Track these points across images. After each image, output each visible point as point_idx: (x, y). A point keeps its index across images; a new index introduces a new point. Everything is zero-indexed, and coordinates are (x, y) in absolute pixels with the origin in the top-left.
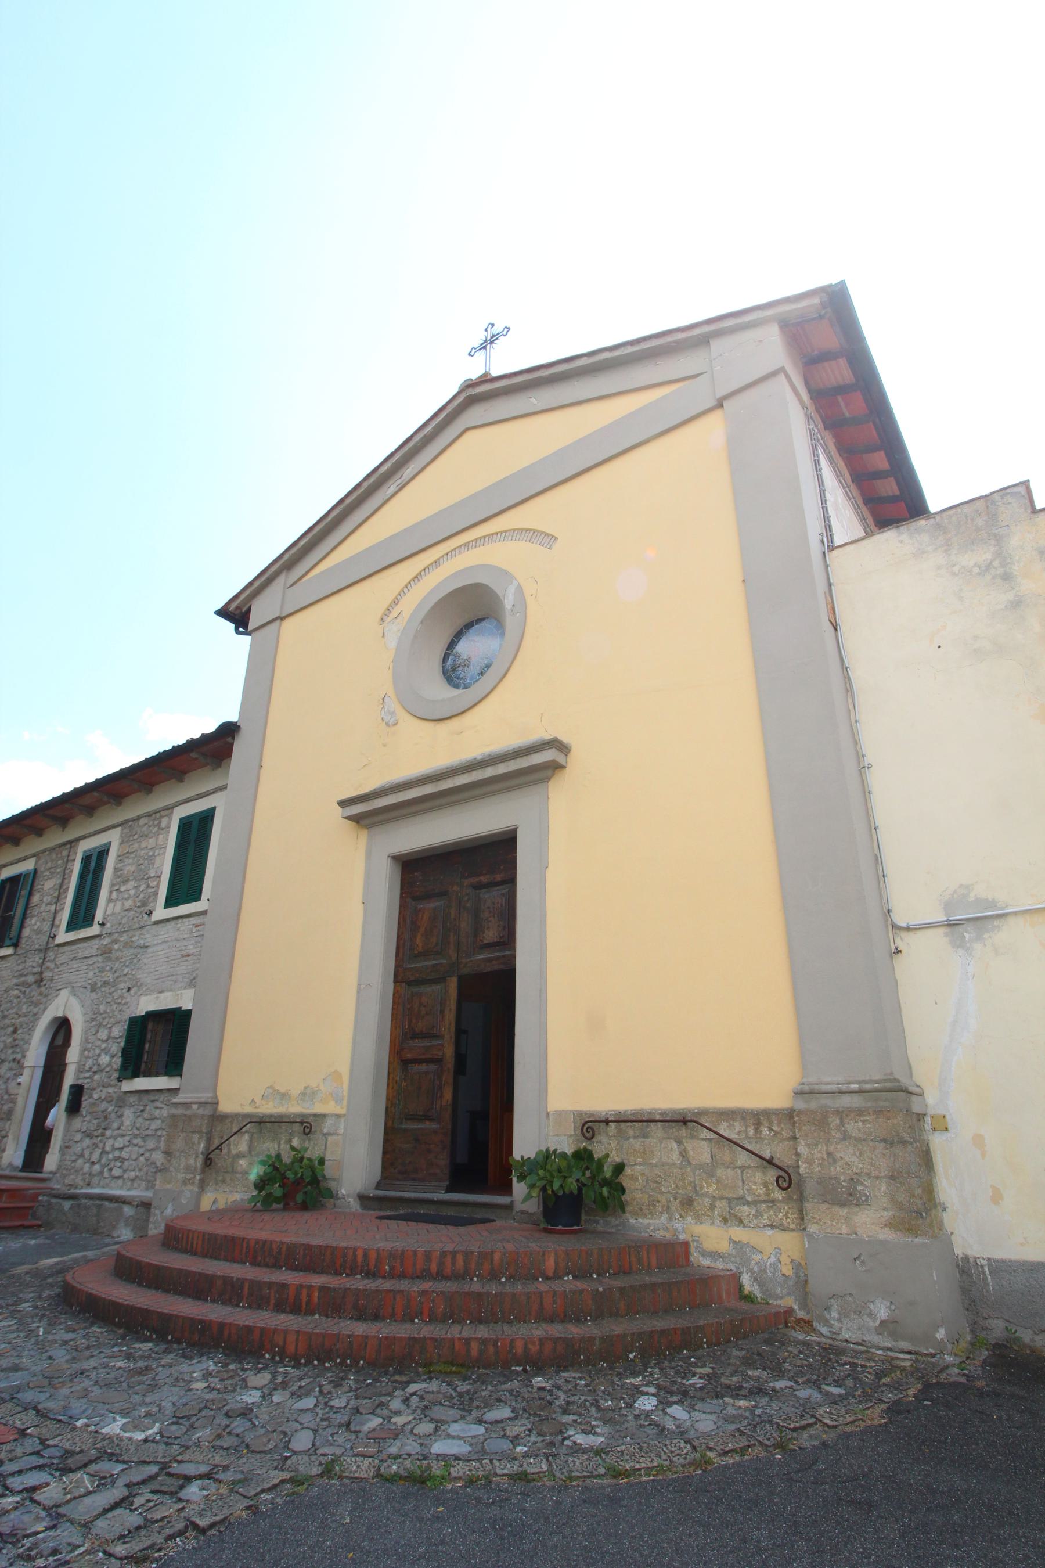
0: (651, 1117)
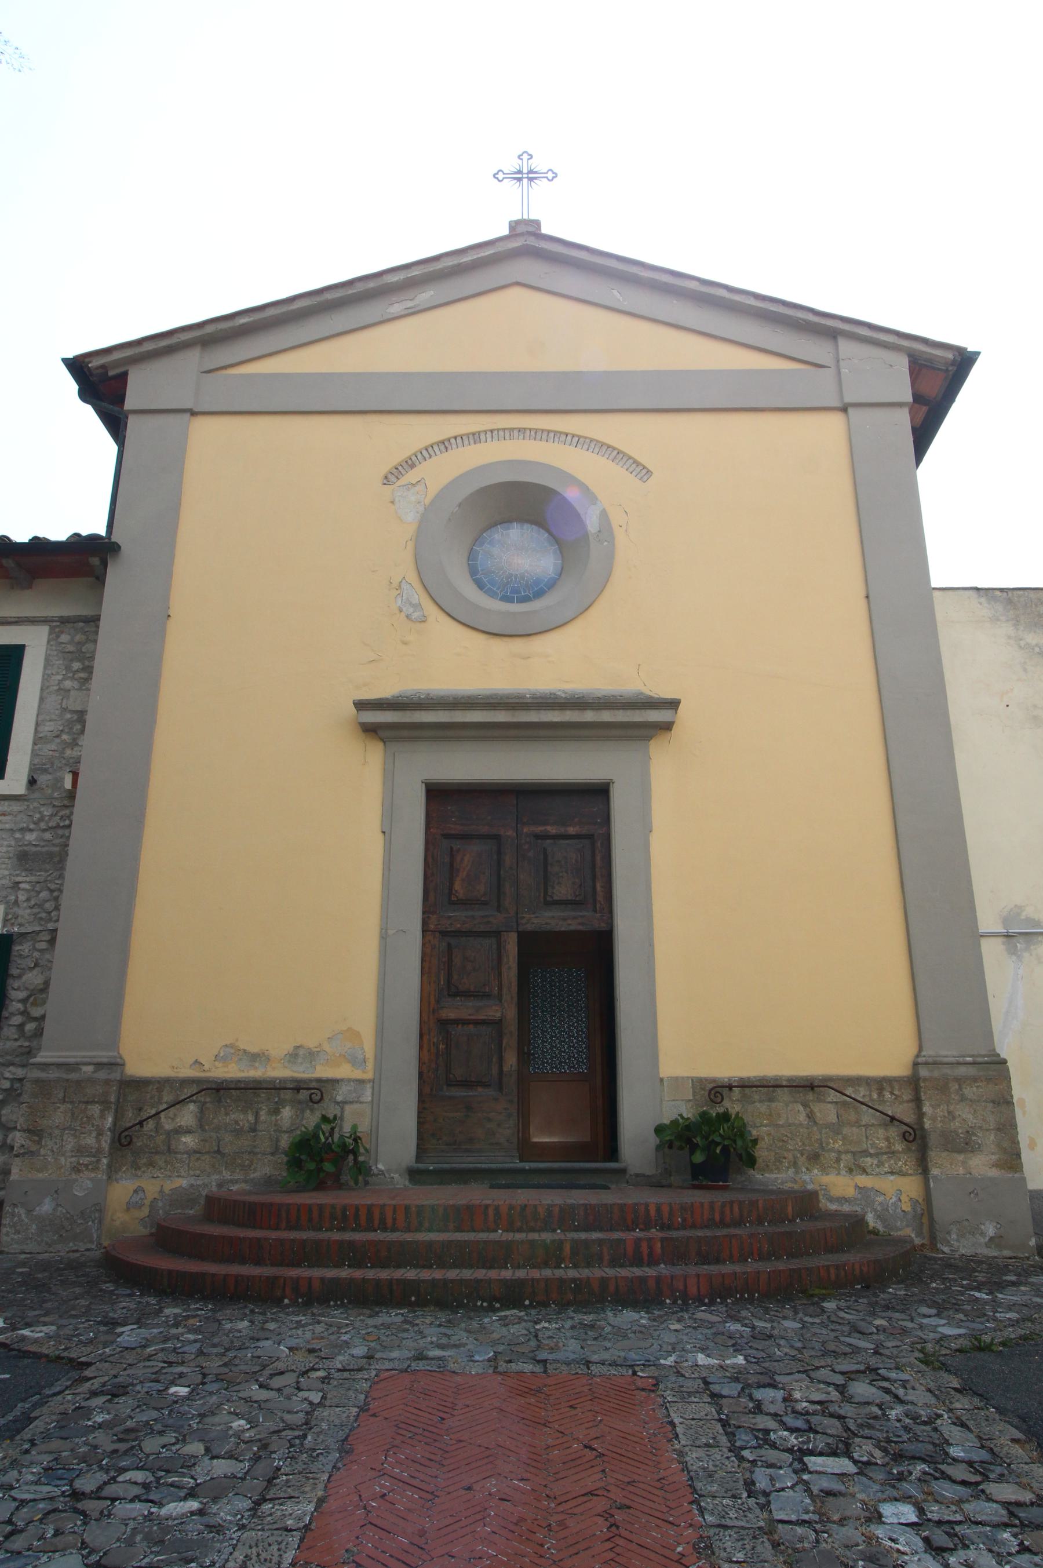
0: (778, 1083)
